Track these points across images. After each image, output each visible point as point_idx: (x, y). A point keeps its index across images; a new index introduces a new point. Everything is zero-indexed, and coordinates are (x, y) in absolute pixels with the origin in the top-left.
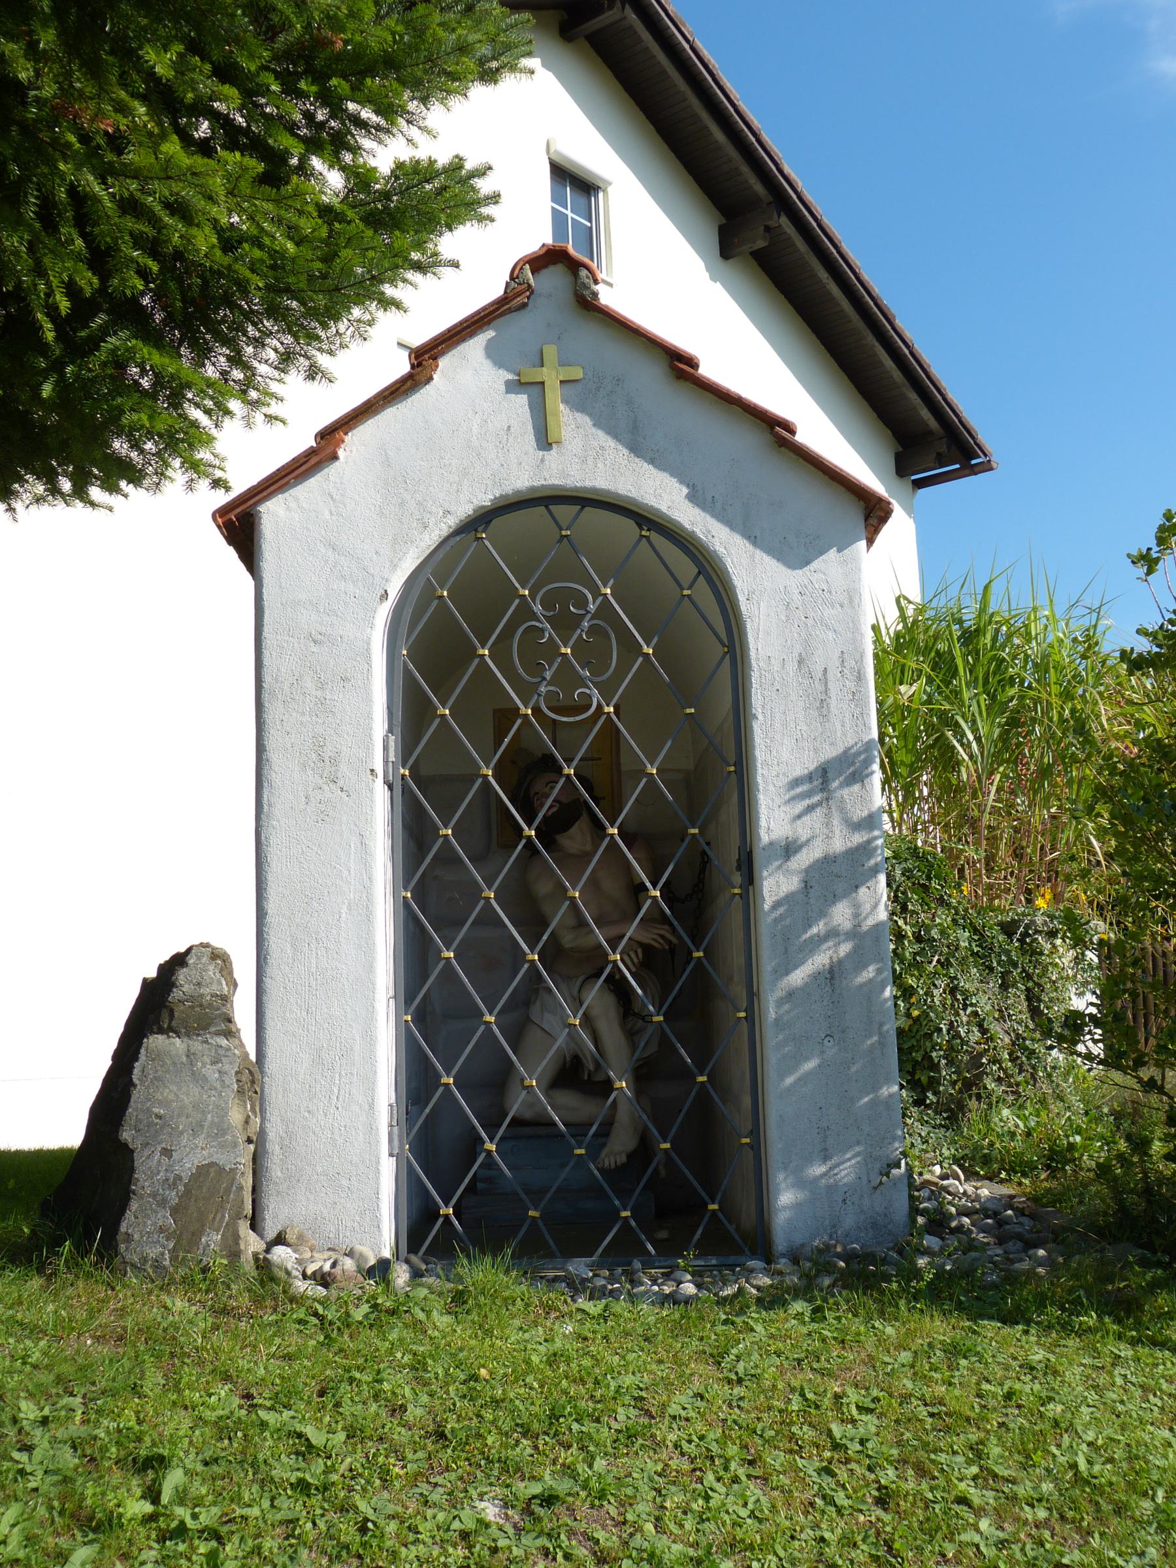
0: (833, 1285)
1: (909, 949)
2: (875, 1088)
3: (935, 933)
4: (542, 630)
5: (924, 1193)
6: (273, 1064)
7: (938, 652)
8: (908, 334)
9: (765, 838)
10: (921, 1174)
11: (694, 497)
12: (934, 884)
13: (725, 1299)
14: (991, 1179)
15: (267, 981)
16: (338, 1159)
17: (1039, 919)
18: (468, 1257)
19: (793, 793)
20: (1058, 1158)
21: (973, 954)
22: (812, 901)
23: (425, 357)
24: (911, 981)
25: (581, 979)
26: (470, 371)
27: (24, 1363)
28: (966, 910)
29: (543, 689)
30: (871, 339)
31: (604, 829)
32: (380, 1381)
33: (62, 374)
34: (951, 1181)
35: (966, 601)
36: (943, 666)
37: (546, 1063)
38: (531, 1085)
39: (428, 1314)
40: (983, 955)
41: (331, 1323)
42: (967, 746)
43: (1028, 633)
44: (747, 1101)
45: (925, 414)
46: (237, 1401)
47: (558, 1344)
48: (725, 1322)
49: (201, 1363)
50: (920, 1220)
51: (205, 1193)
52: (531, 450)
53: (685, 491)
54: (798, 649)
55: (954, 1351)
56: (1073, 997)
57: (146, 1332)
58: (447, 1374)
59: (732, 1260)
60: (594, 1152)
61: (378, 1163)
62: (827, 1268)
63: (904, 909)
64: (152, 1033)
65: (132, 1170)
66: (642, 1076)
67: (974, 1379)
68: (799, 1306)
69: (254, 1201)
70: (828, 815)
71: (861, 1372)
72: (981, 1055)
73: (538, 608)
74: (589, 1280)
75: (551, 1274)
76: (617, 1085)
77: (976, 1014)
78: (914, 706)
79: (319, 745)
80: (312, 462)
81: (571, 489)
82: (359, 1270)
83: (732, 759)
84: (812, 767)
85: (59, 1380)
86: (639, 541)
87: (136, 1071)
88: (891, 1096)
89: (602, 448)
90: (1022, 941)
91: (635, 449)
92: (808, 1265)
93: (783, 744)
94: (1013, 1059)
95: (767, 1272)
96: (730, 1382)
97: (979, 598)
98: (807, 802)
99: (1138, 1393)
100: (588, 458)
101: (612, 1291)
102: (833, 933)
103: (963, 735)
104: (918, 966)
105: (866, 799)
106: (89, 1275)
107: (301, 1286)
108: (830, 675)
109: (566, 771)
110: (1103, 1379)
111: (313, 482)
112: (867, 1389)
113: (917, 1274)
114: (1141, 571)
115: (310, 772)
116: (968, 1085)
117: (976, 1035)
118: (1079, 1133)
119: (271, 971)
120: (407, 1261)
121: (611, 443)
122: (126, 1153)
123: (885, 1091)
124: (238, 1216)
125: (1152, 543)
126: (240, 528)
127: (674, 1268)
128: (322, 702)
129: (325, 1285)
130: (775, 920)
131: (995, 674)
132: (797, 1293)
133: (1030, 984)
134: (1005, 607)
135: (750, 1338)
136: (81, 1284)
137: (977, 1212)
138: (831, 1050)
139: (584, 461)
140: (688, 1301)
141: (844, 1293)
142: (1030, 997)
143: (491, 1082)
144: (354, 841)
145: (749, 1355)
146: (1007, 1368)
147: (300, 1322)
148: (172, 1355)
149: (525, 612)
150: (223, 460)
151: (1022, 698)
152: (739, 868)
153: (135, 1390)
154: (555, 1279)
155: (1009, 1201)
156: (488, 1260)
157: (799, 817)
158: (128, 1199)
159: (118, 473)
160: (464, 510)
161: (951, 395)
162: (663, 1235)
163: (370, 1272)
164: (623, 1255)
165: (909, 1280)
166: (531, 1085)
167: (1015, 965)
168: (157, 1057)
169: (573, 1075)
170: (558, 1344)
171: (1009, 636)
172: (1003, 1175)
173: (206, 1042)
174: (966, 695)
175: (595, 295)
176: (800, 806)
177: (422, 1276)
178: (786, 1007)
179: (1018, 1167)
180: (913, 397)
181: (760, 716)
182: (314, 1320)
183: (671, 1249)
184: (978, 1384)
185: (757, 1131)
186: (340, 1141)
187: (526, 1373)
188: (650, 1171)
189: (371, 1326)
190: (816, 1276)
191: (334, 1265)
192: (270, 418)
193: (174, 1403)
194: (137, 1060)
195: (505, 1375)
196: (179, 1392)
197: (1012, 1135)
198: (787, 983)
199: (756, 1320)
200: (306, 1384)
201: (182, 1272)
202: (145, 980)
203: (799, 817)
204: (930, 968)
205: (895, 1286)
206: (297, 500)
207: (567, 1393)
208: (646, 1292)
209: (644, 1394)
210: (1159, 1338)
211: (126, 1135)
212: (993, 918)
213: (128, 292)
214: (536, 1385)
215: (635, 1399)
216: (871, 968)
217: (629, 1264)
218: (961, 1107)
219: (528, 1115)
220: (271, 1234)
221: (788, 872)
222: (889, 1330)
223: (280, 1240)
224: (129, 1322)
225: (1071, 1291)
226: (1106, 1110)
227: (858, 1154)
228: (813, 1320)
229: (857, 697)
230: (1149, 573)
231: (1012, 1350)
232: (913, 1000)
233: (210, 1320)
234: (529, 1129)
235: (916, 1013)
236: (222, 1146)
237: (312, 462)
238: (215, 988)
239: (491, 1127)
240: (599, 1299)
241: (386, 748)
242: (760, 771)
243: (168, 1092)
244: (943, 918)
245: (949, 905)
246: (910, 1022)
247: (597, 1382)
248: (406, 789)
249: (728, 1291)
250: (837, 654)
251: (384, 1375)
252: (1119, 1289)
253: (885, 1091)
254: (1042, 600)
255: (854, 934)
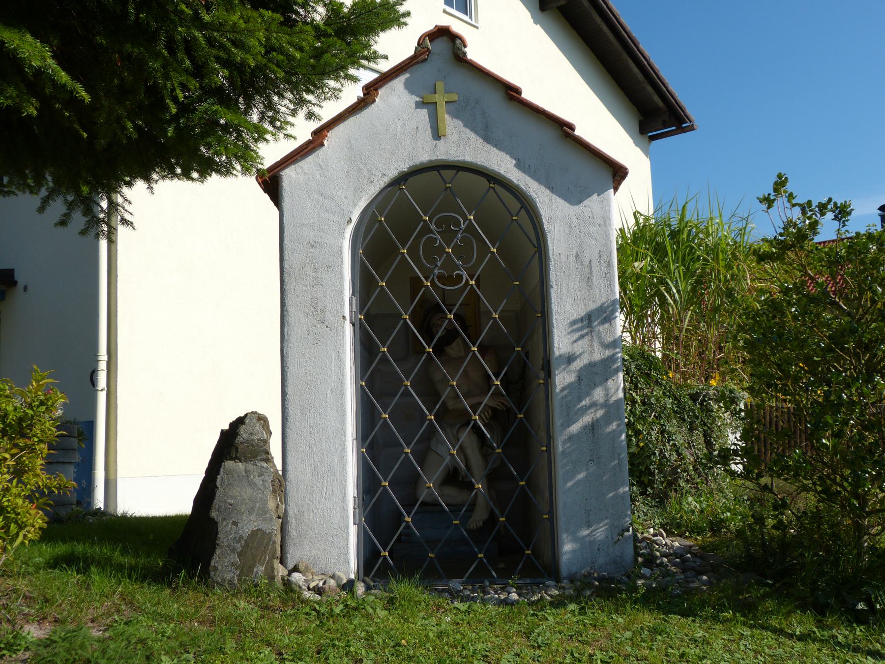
0: (591, 595)
1: (639, 409)
2: (616, 488)
3: (653, 400)
4: (436, 239)
5: (643, 544)
6: (291, 475)
7: (657, 243)
8: (647, 53)
9: (557, 353)
10: (642, 533)
11: (518, 166)
12: (653, 373)
13: (533, 602)
14: (681, 536)
15: (288, 430)
16: (329, 531)
17: (711, 392)
18: (396, 579)
19: (572, 328)
20: (716, 526)
21: (674, 411)
22: (583, 387)
23: (371, 90)
24: (639, 427)
25: (458, 426)
26: (396, 98)
27: (163, 636)
28: (671, 387)
29: (436, 272)
30: (625, 56)
31: (470, 348)
32: (349, 646)
33: (178, 123)
34: (659, 537)
35: (673, 214)
36: (659, 251)
37: (439, 473)
38: (430, 486)
39: (375, 610)
40: (679, 412)
41: (323, 615)
42: (672, 296)
43: (708, 232)
44: (547, 494)
45: (656, 98)
46: (274, 656)
47: (443, 626)
48: (533, 615)
49: (255, 636)
50: (640, 559)
51: (256, 546)
52: (430, 140)
53: (514, 162)
54: (576, 249)
55: (655, 631)
56: (730, 435)
57: (226, 619)
58: (384, 642)
59: (538, 580)
60: (464, 520)
61: (348, 528)
62: (589, 585)
63: (636, 387)
64: (227, 460)
65: (217, 533)
66: (492, 479)
67: (664, 647)
68: (572, 607)
69: (281, 546)
70: (591, 341)
71: (604, 642)
72: (677, 467)
73: (433, 227)
74: (460, 591)
75: (440, 588)
76: (476, 486)
77: (675, 445)
78: (643, 274)
79: (315, 304)
80: (310, 147)
81: (452, 162)
82: (338, 585)
83: (539, 310)
84: (583, 314)
85: (181, 645)
86: (488, 190)
87: (218, 480)
88: (624, 493)
89: (468, 139)
90: (701, 404)
91: (487, 139)
92: (578, 584)
93: (566, 303)
94: (695, 470)
95: (556, 587)
96: (534, 647)
97: (680, 212)
98: (580, 333)
99: (752, 654)
100: (462, 145)
101: (473, 597)
102: (594, 405)
103: (671, 289)
104: (643, 418)
105: (612, 331)
106: (195, 588)
107: (307, 594)
108: (593, 264)
109: (449, 316)
110: (733, 647)
111: (310, 159)
112: (607, 652)
113: (636, 589)
114: (764, 206)
115: (310, 318)
116: (670, 484)
117: (675, 456)
118: (729, 511)
119: (289, 425)
120: (363, 581)
121: (473, 136)
122: (214, 524)
123: (621, 490)
124: (273, 557)
125: (771, 191)
126: (271, 184)
127: (507, 584)
128: (316, 279)
129: (320, 594)
130: (562, 398)
131: (688, 255)
132: (572, 599)
133: (706, 428)
134: (695, 217)
135: (545, 624)
136: (191, 593)
137: (671, 555)
138: (593, 468)
139: (459, 146)
140: (513, 603)
141: (597, 599)
142: (705, 435)
143: (408, 483)
144: (334, 355)
145: (545, 633)
146: (682, 640)
147: (307, 614)
148: (240, 632)
149: (426, 230)
150: (262, 159)
151: (703, 269)
152: (543, 369)
153: (221, 650)
154: (443, 591)
155: (689, 549)
156: (407, 581)
157: (576, 341)
158: (215, 548)
159: (207, 168)
160: (393, 173)
161: (671, 88)
162: (502, 566)
163: (343, 587)
164: (480, 578)
165: (633, 593)
166: (430, 486)
167: (697, 418)
168: (229, 472)
169: (453, 478)
170: (443, 626)
171: (697, 234)
172: (687, 534)
173: (255, 465)
174: (672, 268)
175: (465, 54)
176: (576, 336)
177: (371, 589)
178: (568, 445)
179: (696, 530)
180: (649, 89)
181: (555, 287)
182: (314, 613)
183: (505, 575)
184: (666, 649)
185: (552, 511)
186: (327, 517)
187: (426, 643)
188: (496, 530)
189: (344, 616)
190: (583, 590)
191: (324, 583)
192: (288, 136)
193: (242, 657)
194: (219, 474)
195: (415, 643)
196: (244, 651)
197: (693, 512)
198: (567, 432)
199: (549, 614)
200: (310, 648)
201: (244, 587)
202: (222, 431)
203: (576, 341)
204: (650, 420)
205: (624, 596)
206: (302, 168)
207: (447, 653)
208: (491, 598)
209: (488, 654)
210: (766, 625)
211: (214, 514)
212: (686, 392)
213: (213, 85)
214: (431, 649)
215: (483, 656)
216: (614, 424)
217: (483, 582)
218: (666, 496)
219: (429, 500)
220: (291, 566)
221: (570, 371)
222: (620, 620)
223: (296, 569)
224: (217, 614)
225: (720, 599)
226: (746, 498)
227: (606, 524)
228: (580, 614)
229: (608, 276)
230: (769, 208)
231: (686, 631)
232: (640, 437)
233: (260, 613)
234: (430, 506)
235: (642, 444)
236: (264, 520)
237: (310, 147)
238: (260, 436)
239: (408, 507)
240: (466, 602)
241: (351, 304)
242: (554, 316)
243: (235, 492)
244: (658, 392)
245: (661, 384)
246: (639, 449)
247: (463, 647)
248: (361, 324)
249: (535, 598)
250: (597, 251)
251: (351, 643)
252: (746, 598)
253: (621, 490)
254: (716, 213)
255: (606, 405)
